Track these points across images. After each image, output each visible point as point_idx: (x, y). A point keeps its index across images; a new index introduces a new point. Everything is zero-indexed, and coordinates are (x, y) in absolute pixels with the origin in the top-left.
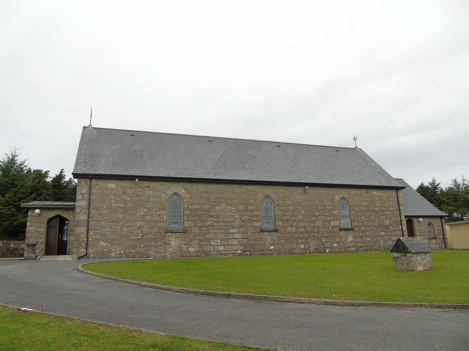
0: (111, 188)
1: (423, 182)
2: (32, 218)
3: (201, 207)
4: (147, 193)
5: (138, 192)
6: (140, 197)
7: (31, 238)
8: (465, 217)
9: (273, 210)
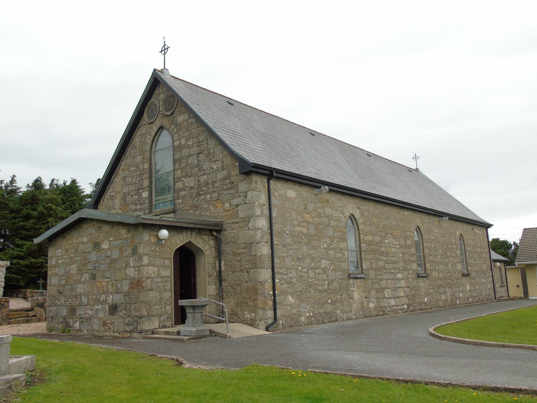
0: (291, 198)
1: (14, 176)
2: (151, 247)
3: (373, 239)
4: (328, 211)
5: (318, 209)
6: (321, 217)
7: (151, 290)
8: (517, 262)
9: (421, 247)
